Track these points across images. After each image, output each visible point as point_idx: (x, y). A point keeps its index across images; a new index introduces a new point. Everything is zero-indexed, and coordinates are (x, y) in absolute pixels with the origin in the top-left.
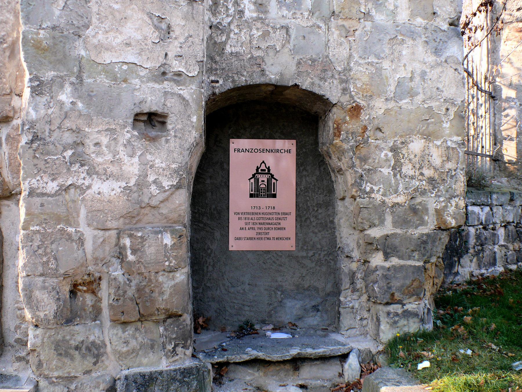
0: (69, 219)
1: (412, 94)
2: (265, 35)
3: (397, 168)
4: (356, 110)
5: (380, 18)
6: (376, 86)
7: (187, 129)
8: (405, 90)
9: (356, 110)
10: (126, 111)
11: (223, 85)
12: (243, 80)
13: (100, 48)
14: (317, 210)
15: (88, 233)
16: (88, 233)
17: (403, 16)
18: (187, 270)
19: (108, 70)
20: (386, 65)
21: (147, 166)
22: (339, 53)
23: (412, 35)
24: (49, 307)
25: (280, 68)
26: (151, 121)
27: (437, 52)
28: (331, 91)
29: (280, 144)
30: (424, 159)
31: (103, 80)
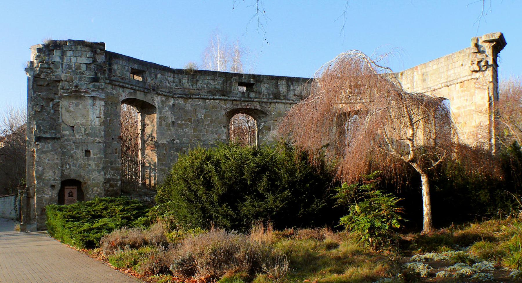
0: (42, 200)
1: (95, 180)
3: (92, 192)
4: (85, 183)
5: (90, 168)
6: (89, 178)
7: (58, 187)
8: (93, 179)
9: (85, 183)
11: (64, 179)
12: (67, 178)
13: (46, 177)
17: (94, 167)
18: (250, 118)
19: (47, 180)
20: (91, 176)
21: (52, 193)
22: (83, 174)
23: (95, 170)
24: (39, 213)
25: (73, 176)
26: (53, 187)
27: (99, 173)
28: (81, 180)
29: (74, 187)
30: (97, 191)
31: (46, 181)
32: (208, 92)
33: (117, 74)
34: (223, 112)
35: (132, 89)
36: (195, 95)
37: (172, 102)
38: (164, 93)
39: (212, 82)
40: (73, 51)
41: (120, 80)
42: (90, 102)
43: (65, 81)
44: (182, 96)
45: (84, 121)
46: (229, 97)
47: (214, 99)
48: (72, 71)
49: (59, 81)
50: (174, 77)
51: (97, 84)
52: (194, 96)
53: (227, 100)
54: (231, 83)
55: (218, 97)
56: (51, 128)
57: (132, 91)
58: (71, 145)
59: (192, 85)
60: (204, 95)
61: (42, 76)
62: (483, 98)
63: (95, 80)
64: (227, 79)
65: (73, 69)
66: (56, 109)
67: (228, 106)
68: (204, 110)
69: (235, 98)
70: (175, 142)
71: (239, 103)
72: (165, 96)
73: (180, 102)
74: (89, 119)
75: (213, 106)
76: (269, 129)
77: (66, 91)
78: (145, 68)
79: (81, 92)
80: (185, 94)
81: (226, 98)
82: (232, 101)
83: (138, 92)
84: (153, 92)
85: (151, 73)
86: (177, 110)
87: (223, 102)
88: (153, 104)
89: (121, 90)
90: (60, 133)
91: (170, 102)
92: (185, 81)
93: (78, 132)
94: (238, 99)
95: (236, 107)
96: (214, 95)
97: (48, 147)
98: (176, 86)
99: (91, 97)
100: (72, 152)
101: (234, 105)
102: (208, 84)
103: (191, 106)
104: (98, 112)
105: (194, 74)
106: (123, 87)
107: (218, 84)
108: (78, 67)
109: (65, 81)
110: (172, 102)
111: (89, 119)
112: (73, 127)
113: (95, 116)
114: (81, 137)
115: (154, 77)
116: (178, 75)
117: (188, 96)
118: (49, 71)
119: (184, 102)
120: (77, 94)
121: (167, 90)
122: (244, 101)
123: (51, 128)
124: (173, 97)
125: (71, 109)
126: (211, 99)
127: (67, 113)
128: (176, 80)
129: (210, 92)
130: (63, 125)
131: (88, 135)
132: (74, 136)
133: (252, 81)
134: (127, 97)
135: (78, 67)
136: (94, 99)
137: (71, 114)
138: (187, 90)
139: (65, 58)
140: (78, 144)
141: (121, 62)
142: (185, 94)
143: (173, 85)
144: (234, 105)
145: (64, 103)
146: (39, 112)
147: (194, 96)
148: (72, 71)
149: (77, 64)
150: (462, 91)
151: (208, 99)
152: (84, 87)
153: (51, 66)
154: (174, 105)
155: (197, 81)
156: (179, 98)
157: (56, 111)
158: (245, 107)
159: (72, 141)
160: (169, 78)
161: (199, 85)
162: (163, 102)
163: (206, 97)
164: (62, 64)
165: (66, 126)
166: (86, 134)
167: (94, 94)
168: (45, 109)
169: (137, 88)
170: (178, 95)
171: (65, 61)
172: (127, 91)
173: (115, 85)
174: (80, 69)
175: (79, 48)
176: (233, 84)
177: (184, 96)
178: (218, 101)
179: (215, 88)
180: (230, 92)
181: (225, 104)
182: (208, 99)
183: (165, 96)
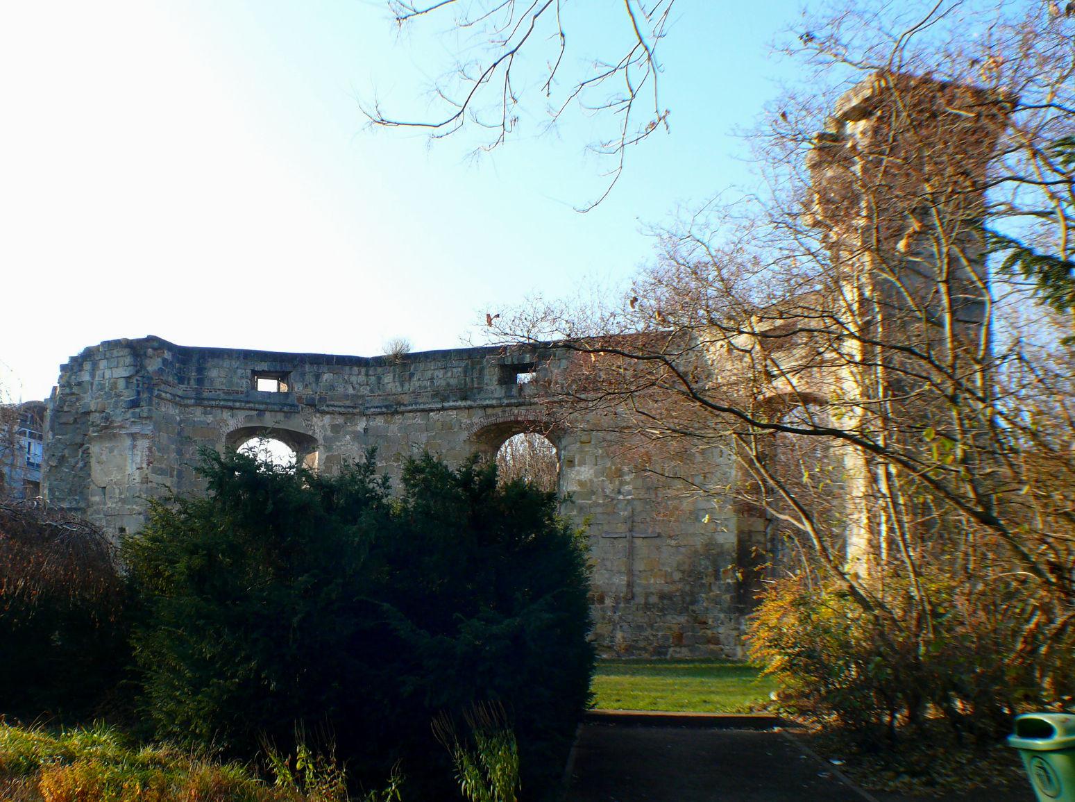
32: (434, 396)
33: (217, 385)
34: (464, 435)
35: (251, 409)
36: (405, 405)
37: (361, 425)
38: (337, 409)
39: (440, 374)
40: (107, 359)
41: (222, 396)
42: (128, 442)
43: (95, 411)
44: (379, 410)
46: (475, 401)
47: (443, 409)
48: (106, 393)
49: (88, 413)
50: (367, 375)
51: (137, 410)
52: (403, 408)
53: (470, 408)
54: (481, 370)
55: (451, 404)
56: (71, 492)
57: (255, 413)
58: (101, 519)
59: (402, 386)
60: (425, 402)
61: (66, 409)
63: (134, 404)
64: (472, 363)
65: (107, 389)
67: (475, 420)
68: (425, 435)
69: (487, 402)
71: (498, 411)
72: (340, 414)
73: (379, 421)
74: (127, 473)
75: (443, 424)
76: (571, 463)
78: (288, 367)
79: (114, 428)
80: (386, 407)
81: (469, 403)
82: (485, 407)
83: (267, 414)
84: (309, 410)
85: (303, 374)
87: (465, 413)
88: (310, 433)
89: (226, 414)
90: (87, 500)
91: (357, 424)
92: (388, 379)
93: (111, 497)
94: (494, 402)
95: (492, 420)
96: (443, 401)
98: (372, 391)
99: (128, 434)
102: (432, 379)
103: (400, 429)
104: (138, 459)
105: (404, 362)
106: (231, 408)
107: (453, 376)
108: (114, 386)
109: (95, 411)
110: (361, 425)
111: (127, 473)
112: (105, 488)
113: (135, 467)
114: (114, 505)
115: (312, 379)
116: (376, 370)
117: (392, 409)
118: (73, 398)
119: (386, 421)
121: (348, 403)
122: (508, 405)
123: (71, 492)
124: (363, 414)
125: (104, 458)
126: (439, 410)
128: (373, 379)
129: (436, 395)
130: (92, 486)
131: (123, 501)
132: (105, 504)
134: (240, 426)
135: (114, 386)
136: (134, 436)
138: (391, 398)
139: (97, 373)
141: (226, 363)
142: (386, 407)
143: (365, 391)
144: (488, 417)
145: (95, 449)
146: (56, 467)
147: (403, 408)
148: (106, 393)
149: (112, 381)
151: (431, 410)
152: (120, 419)
153: (75, 390)
154: (366, 430)
155: (411, 375)
157: (87, 464)
158: (512, 418)
160: (353, 379)
161: (415, 383)
162: (335, 428)
163: (427, 406)
164: (92, 384)
166: (121, 500)
167: (135, 429)
168: (68, 462)
169: (262, 407)
170: (372, 410)
171: (97, 378)
172: (241, 415)
173: (212, 407)
174: (116, 388)
175: (115, 353)
176: (486, 371)
177: (384, 410)
178: (455, 412)
179: (448, 384)
180: (480, 389)
181: (470, 417)
182: (431, 410)
183: (340, 414)
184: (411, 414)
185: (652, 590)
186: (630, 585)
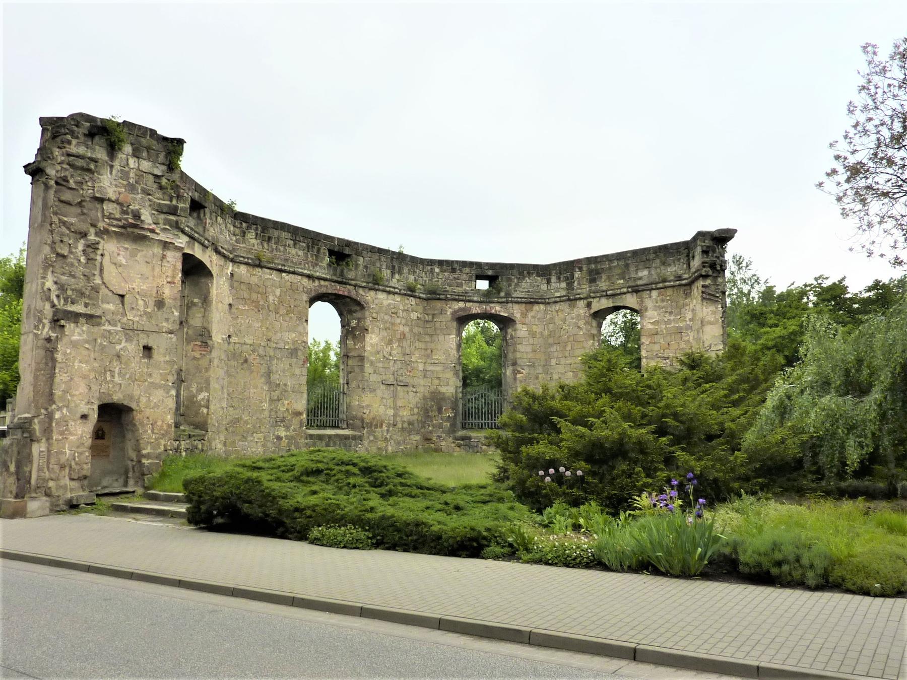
2: (114, 387)
10: (79, 415)
14: (375, 437)
15: (68, 452)
16: (68, 452)
21: (83, 431)
22: (136, 393)
26: (84, 417)
28: (133, 405)
45: (144, 287)
62: (714, 313)
66: (92, 255)
70: (232, 340)
77: (115, 222)
79: (143, 229)
86: (236, 284)
97: (80, 334)
100: (118, 347)
101: (320, 286)
112: (122, 296)
114: (137, 319)
120: (132, 232)
127: (113, 267)
130: (104, 291)
133: (347, 251)
137: (120, 269)
140: (131, 333)
150: (663, 300)
151: (285, 271)
156: (241, 263)
159: (119, 325)
165: (110, 294)
166: (146, 313)
178: (300, 277)
184: (268, 271)
185: (405, 419)
186: (394, 416)
